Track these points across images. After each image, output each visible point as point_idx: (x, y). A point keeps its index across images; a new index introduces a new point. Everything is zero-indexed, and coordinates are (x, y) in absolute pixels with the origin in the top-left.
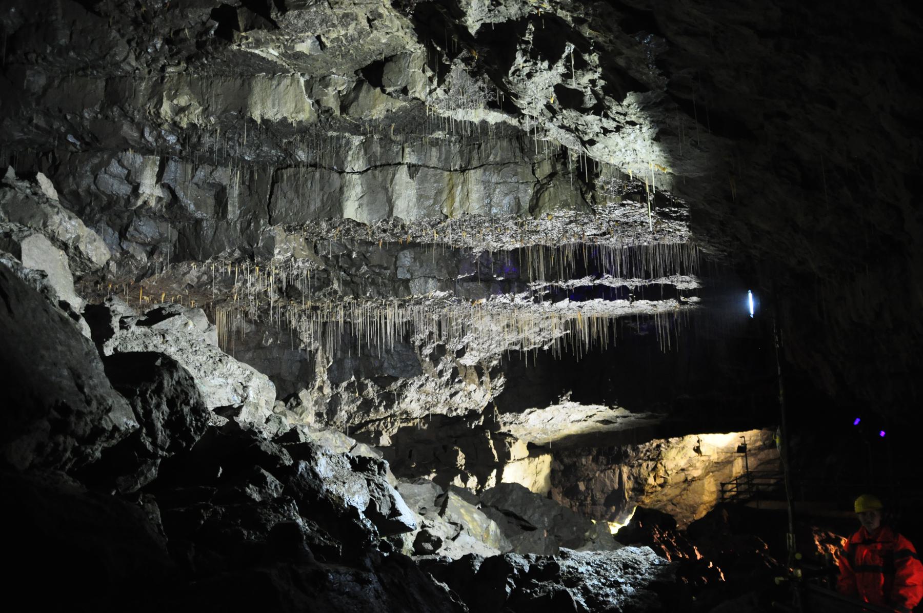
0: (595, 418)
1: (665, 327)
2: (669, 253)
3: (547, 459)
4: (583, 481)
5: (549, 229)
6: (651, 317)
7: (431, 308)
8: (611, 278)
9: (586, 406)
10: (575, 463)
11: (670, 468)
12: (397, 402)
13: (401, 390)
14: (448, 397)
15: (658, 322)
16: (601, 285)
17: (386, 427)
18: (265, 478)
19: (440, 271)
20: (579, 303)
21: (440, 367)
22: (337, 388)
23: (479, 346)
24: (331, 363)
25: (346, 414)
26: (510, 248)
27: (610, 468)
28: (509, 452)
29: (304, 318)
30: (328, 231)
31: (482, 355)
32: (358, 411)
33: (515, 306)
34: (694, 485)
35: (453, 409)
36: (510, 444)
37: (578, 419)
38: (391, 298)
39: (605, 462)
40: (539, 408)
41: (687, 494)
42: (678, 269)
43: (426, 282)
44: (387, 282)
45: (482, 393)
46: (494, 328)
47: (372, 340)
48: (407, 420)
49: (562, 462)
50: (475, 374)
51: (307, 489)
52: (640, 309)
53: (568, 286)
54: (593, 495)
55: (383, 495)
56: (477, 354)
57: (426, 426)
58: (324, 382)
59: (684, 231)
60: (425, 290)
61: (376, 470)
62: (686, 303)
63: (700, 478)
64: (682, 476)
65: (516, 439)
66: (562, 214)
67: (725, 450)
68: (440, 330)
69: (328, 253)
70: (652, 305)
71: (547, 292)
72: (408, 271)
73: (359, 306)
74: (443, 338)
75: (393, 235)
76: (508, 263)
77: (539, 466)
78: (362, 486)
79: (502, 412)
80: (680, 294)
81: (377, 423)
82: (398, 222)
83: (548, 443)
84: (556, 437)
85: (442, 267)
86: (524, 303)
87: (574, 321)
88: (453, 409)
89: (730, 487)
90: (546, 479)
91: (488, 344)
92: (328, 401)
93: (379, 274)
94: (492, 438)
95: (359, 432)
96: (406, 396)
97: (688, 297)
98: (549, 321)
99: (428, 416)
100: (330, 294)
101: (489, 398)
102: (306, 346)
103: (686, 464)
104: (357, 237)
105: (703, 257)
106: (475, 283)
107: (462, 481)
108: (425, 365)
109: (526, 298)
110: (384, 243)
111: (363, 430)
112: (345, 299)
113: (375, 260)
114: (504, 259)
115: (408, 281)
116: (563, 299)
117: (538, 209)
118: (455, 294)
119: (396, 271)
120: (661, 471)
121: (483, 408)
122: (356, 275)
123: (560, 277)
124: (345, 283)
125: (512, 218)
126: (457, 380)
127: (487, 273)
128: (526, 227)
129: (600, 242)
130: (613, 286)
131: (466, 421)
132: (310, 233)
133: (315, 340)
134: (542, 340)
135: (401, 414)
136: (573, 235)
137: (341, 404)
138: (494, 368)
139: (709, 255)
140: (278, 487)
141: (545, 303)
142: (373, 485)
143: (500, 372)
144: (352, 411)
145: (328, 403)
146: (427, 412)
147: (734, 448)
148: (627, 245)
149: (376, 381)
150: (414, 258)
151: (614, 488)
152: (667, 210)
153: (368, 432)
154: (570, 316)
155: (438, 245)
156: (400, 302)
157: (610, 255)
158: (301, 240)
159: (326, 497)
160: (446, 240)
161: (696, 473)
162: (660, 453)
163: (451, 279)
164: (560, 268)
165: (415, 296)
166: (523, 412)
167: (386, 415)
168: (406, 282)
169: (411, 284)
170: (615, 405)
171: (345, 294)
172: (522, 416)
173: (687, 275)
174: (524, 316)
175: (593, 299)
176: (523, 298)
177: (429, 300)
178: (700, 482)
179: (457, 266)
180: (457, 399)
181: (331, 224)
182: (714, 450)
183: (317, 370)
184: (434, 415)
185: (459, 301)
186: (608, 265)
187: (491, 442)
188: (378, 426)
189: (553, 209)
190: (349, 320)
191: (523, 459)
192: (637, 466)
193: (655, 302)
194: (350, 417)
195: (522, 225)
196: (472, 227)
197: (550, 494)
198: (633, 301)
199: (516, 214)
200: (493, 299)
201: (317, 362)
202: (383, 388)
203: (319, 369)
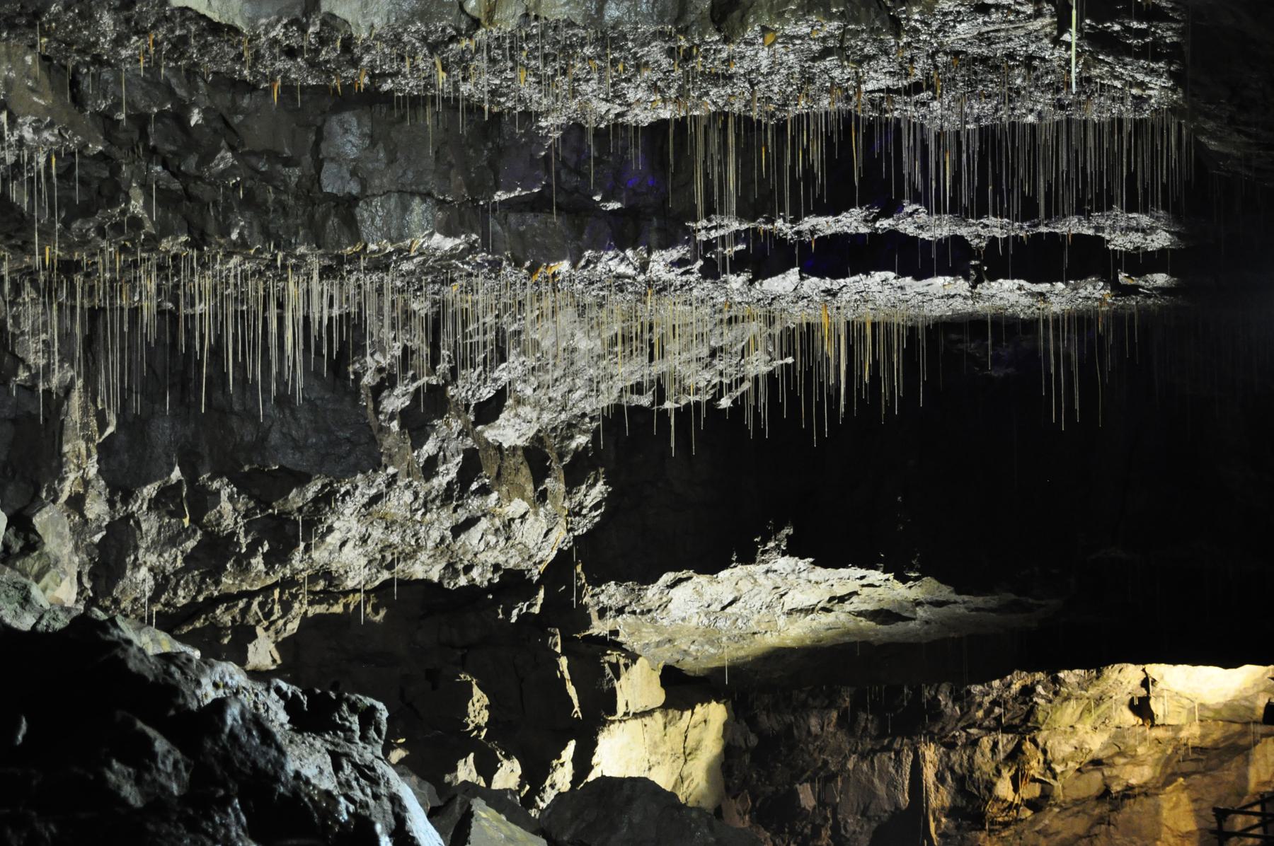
0: (856, 604)
1: (1068, 357)
2: (1099, 146)
3: (715, 713)
4: (811, 780)
5: (764, 70)
7: (414, 284)
8: (923, 217)
10: (789, 728)
11: (1059, 756)
12: (302, 545)
13: (318, 511)
14: (448, 533)
15: (1049, 343)
16: (893, 234)
17: (268, 615)
19: (446, 176)
20: (827, 283)
21: (429, 448)
22: (125, 502)
23: (540, 393)
24: (110, 430)
26: (643, 117)
27: (888, 749)
28: (614, 690)
29: (28, 294)
30: (119, 41)
31: (546, 417)
32: (186, 570)
33: (649, 283)
35: (460, 567)
36: (615, 668)
38: (301, 250)
40: (700, 572)
42: (1122, 193)
43: (405, 208)
46: (583, 344)
47: (241, 367)
48: (328, 596)
49: (752, 723)
50: (525, 471)
52: (999, 303)
53: (799, 233)
56: (535, 415)
57: (382, 613)
58: (86, 483)
59: (1158, 89)
65: (633, 657)
66: (804, 29)
67: (1226, 714)
68: (435, 347)
69: (116, 106)
70: (1032, 294)
71: (741, 247)
72: (353, 173)
74: (443, 367)
75: (312, 64)
76: (637, 159)
77: (693, 735)
79: (597, 580)
80: (1118, 265)
81: (241, 604)
82: (334, 29)
83: (720, 670)
84: (742, 653)
85: (451, 166)
86: (674, 276)
88: (460, 567)
89: (1239, 822)
90: (710, 770)
92: (97, 538)
93: (268, 178)
96: (330, 529)
98: (737, 329)
99: (387, 584)
100: (117, 228)
101: (560, 537)
102: (34, 377)
103: (1105, 747)
104: (207, 65)
105: (1201, 160)
106: (542, 217)
108: (388, 442)
109: (680, 263)
110: (288, 89)
112: (165, 244)
113: (258, 134)
114: (625, 149)
115: (352, 201)
116: (782, 269)
117: (737, 14)
118: (485, 244)
120: (1034, 763)
121: (542, 567)
122: (200, 178)
123: (782, 209)
124: (167, 199)
125: (661, 35)
126: (474, 486)
127: (576, 189)
128: (698, 64)
130: (925, 235)
131: (495, 603)
132: (59, 42)
133: (61, 361)
134: (716, 380)
135: (313, 579)
136: (829, 91)
137: (136, 548)
138: (579, 454)
139: (1227, 156)
141: (732, 278)
143: (595, 468)
144: (169, 568)
145: (98, 545)
146: (385, 575)
147: (1252, 710)
148: (978, 119)
149: (243, 484)
150: (371, 137)
151: (897, 807)
152: (1117, 28)
153: (215, 629)
154: (798, 315)
155: (446, 101)
156: (327, 262)
157: (925, 148)
158: (29, 59)
160: (465, 88)
161: (1138, 775)
162: (1031, 711)
163: (475, 201)
165: (372, 247)
166: (655, 580)
167: (269, 582)
169: (362, 212)
170: (912, 569)
171: (165, 230)
172: (652, 593)
173: (1145, 211)
174: (670, 311)
175: (867, 273)
176: (673, 264)
177: (409, 259)
180: (473, 538)
181: (128, 20)
182: (1191, 711)
183: (66, 448)
184: (408, 584)
185: (495, 266)
186: (918, 178)
187: (563, 662)
189: (780, 15)
190: (170, 305)
191: (648, 713)
192: (964, 746)
193: (1044, 287)
194: (163, 583)
195: (688, 56)
196: (546, 56)
197: (718, 812)
198: (979, 280)
199: (675, 22)
200: (588, 262)
201: (69, 422)
202: (264, 503)
203: (73, 446)
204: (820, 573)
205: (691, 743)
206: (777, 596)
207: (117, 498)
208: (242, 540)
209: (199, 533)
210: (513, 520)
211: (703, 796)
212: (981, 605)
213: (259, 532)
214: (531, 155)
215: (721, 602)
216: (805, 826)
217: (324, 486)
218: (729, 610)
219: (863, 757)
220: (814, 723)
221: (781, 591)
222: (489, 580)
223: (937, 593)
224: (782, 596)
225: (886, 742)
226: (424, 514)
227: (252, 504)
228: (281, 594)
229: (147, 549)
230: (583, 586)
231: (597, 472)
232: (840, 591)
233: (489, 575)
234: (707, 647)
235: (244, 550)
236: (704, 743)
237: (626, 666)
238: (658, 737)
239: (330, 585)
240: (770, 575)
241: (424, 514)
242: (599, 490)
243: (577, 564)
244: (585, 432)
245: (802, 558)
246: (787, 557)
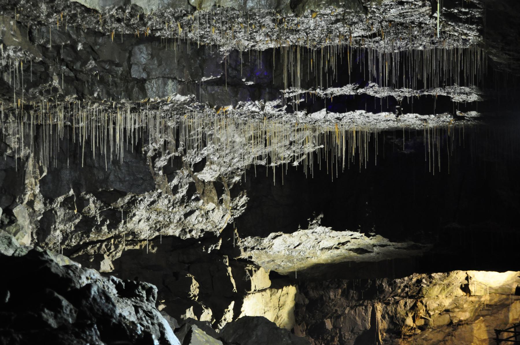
0: (349, 246)
2: (449, 59)
3: (291, 290)
4: (330, 318)
5: (312, 28)
6: (419, 133)
7: (169, 115)
8: (376, 88)
10: (322, 296)
11: (432, 308)
12: (123, 221)
14: (183, 217)
15: (428, 139)
16: (364, 95)
17: (109, 250)
18: (60, 301)
19: (182, 71)
20: (337, 115)
21: (175, 182)
22: (51, 203)
23: (220, 159)
24: (45, 174)
25: (60, 234)
27: (362, 305)
28: (250, 281)
29: (11, 118)
30: (49, 16)
31: (223, 169)
32: (75, 231)
33: (265, 115)
34: (461, 330)
35: (187, 230)
36: (251, 272)
38: (123, 101)
39: (355, 297)
41: (452, 340)
43: (165, 84)
44: (119, 81)
45: (221, 213)
46: (238, 139)
47: (98, 149)
48: (133, 242)
49: (307, 294)
50: (214, 191)
51: (100, 313)
52: (408, 123)
53: (326, 94)
54: (341, 335)
55: (153, 324)
56: (218, 168)
57: (156, 249)
58: (35, 196)
59: (473, 36)
60: (163, 92)
61: (145, 295)
62: (463, 118)
63: (467, 322)
64: (446, 318)
65: (258, 267)
66: (328, 11)
67: (500, 291)
68: (177, 141)
69: (48, 42)
70: (421, 120)
71: (302, 100)
72: (144, 70)
73: (83, 107)
74: (181, 149)
75: (128, 25)
76: (260, 64)
77: (282, 299)
78: (130, 314)
80: (456, 108)
81: (98, 245)
83: (293, 273)
84: (302, 266)
85: (184, 66)
86: (275, 112)
87: (330, 134)
88: (187, 230)
90: (289, 314)
91: (230, 157)
92: (39, 218)
93: (109, 72)
94: (230, 265)
96: (134, 215)
97: (465, 111)
98: (301, 134)
99: (157, 237)
100: (48, 92)
101: (228, 218)
102: (14, 152)
104: (85, 26)
105: (490, 65)
106: (221, 87)
108: (158, 179)
109: (278, 106)
110: (118, 35)
112: (67, 98)
113: (105, 54)
116: (319, 109)
118: (198, 99)
119: (130, 69)
120: (421, 311)
121: (221, 231)
122: (82, 71)
123: (319, 85)
124: (68, 80)
125: (270, 13)
126: (193, 197)
127: (235, 77)
128: (285, 25)
129: (368, 44)
130: (378, 96)
131: (202, 245)
133: (25, 146)
134: (292, 154)
135: (127, 235)
136: (338, 37)
137: (55, 222)
138: (236, 185)
139: (501, 64)
140: (73, 311)
141: (299, 113)
142: (141, 312)
143: (242, 190)
144: (69, 231)
145: (39, 221)
146: (157, 234)
148: (399, 48)
149: (99, 196)
150: (152, 55)
151: (366, 329)
152: (456, 11)
153: (87, 256)
154: (326, 128)
156: (133, 106)
159: (120, 322)
160: (190, 35)
161: (464, 316)
162: (420, 290)
163: (194, 81)
164: (319, 73)
166: (267, 236)
167: (109, 236)
168: (141, 83)
169: (148, 85)
170: (372, 232)
171: (67, 93)
172: (266, 241)
173: (467, 86)
174: (273, 126)
175: (354, 111)
176: (275, 107)
177: (167, 104)
178: (469, 326)
179: (201, 66)
182: (486, 290)
184: (166, 237)
185: (202, 108)
186: (375, 72)
187: (229, 269)
189: (319, 6)
190: (69, 123)
191: (264, 290)
192: (393, 304)
193: (426, 117)
194: (66, 237)
195: (281, 22)
196: (223, 22)
197: (293, 331)
198: (400, 114)
199: (276, 8)
200: (240, 106)
202: (107, 204)
203: (29, 181)
204: (334, 233)
205: (281, 302)
206: (317, 242)
208: (98, 219)
209: (81, 216)
210: (209, 211)
211: (286, 324)
213: (105, 216)
215: (294, 245)
216: (328, 337)
218: (297, 248)
220: (332, 295)
221: (319, 240)
222: (199, 236)
224: (319, 242)
225: (361, 302)
226: (173, 209)
228: (114, 241)
229: (60, 223)
230: (237, 238)
231: (244, 192)
232: (342, 241)
233: (199, 234)
235: (99, 223)
236: (287, 303)
237: (255, 271)
238: (268, 300)
239: (134, 238)
240: (314, 234)
242: (244, 199)
243: (235, 229)
244: (238, 175)
245: (327, 227)
246: (321, 227)
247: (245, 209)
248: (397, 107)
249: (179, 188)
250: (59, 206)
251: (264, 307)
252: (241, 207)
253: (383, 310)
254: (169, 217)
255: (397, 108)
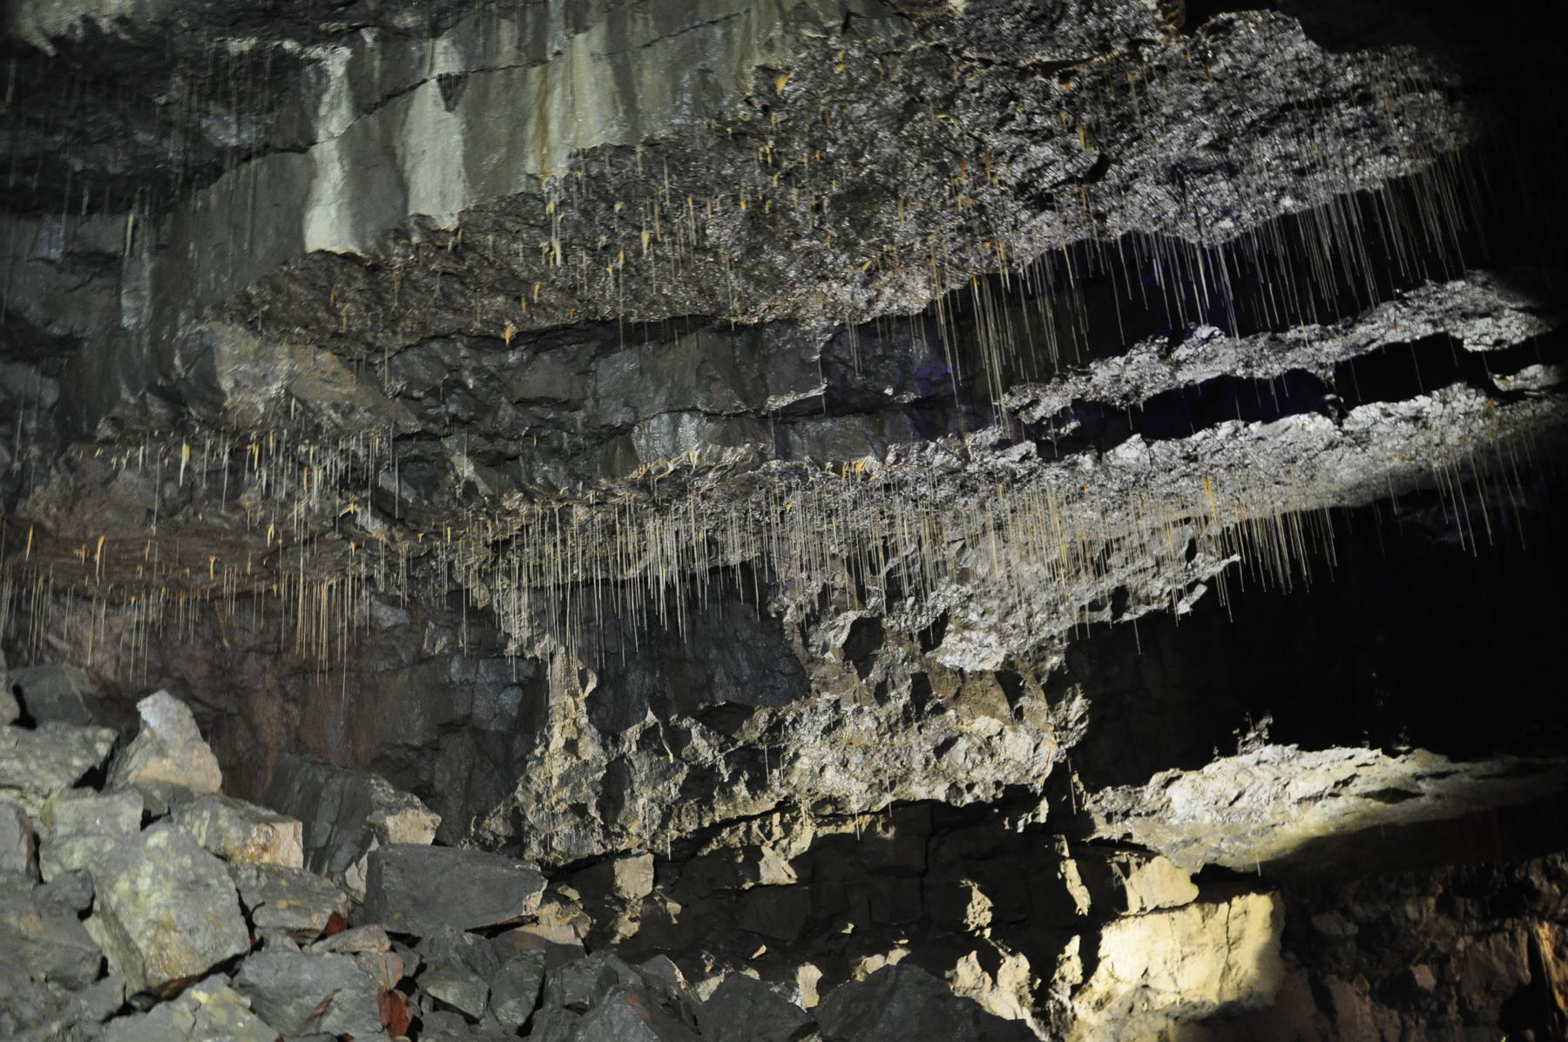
0: (1358, 786)
3: (1258, 907)
4: (1424, 961)
9: (1316, 753)
10: (1386, 916)
14: (931, 754)
17: (769, 835)
21: (875, 675)
27: (1500, 929)
35: (963, 786)
36: (1126, 869)
37: (1313, 792)
40: (1188, 767)
43: (675, 425)
84: (1275, 847)
88: (963, 786)
92: (599, 775)
95: (706, 852)
96: (797, 756)
101: (1051, 752)
107: (984, 968)
111: (714, 846)
115: (626, 430)
121: (1042, 780)
131: (1001, 816)
137: (631, 782)
138: (1055, 675)
166: (1147, 782)
170: (1401, 742)
172: (1149, 792)
183: (552, 703)
188: (748, 832)
191: (1184, 907)
204: (1310, 758)
205: (1233, 934)
206: (1280, 787)
207: (609, 742)
208: (723, 771)
209: (686, 768)
210: (990, 738)
211: (1257, 982)
212: (1485, 772)
213: (737, 763)
214: (801, 360)
215: (1227, 798)
216: (1431, 1004)
217: (771, 716)
218: (1238, 805)
219: (1478, 936)
220: (1411, 911)
221: (1283, 780)
222: (994, 796)
223: (1434, 764)
224: (1285, 786)
225: (1496, 923)
226: (892, 737)
227: (722, 739)
228: (782, 817)
229: (642, 783)
230: (1081, 794)
231: (1074, 689)
232: (1343, 776)
233: (993, 792)
234: (1238, 844)
235: (726, 780)
236: (1247, 933)
237: (1139, 865)
238: (1193, 929)
239: (837, 809)
240: (1262, 765)
241: (892, 737)
242: (1078, 705)
243: (1073, 774)
244: (1057, 653)
245: (1286, 744)
246: (1271, 746)
247: (1088, 727)
248: (1329, 397)
249: (890, 687)
250: (634, 748)
251: (1178, 946)
252: (1076, 724)
253: (1556, 937)
254: (897, 758)
255: (1331, 401)
